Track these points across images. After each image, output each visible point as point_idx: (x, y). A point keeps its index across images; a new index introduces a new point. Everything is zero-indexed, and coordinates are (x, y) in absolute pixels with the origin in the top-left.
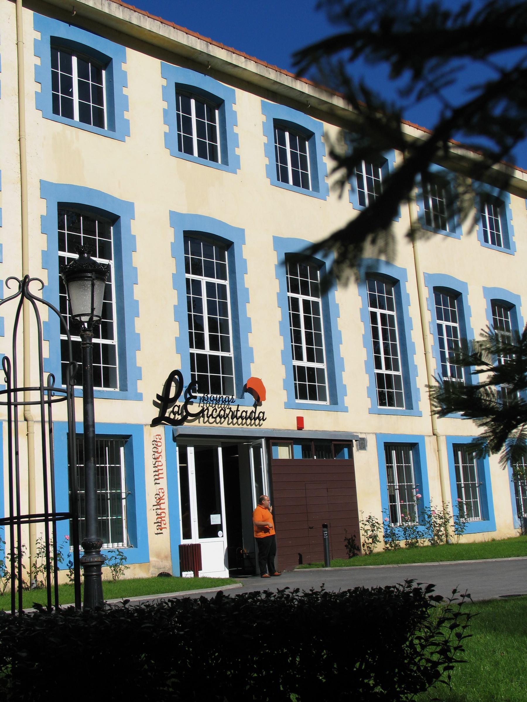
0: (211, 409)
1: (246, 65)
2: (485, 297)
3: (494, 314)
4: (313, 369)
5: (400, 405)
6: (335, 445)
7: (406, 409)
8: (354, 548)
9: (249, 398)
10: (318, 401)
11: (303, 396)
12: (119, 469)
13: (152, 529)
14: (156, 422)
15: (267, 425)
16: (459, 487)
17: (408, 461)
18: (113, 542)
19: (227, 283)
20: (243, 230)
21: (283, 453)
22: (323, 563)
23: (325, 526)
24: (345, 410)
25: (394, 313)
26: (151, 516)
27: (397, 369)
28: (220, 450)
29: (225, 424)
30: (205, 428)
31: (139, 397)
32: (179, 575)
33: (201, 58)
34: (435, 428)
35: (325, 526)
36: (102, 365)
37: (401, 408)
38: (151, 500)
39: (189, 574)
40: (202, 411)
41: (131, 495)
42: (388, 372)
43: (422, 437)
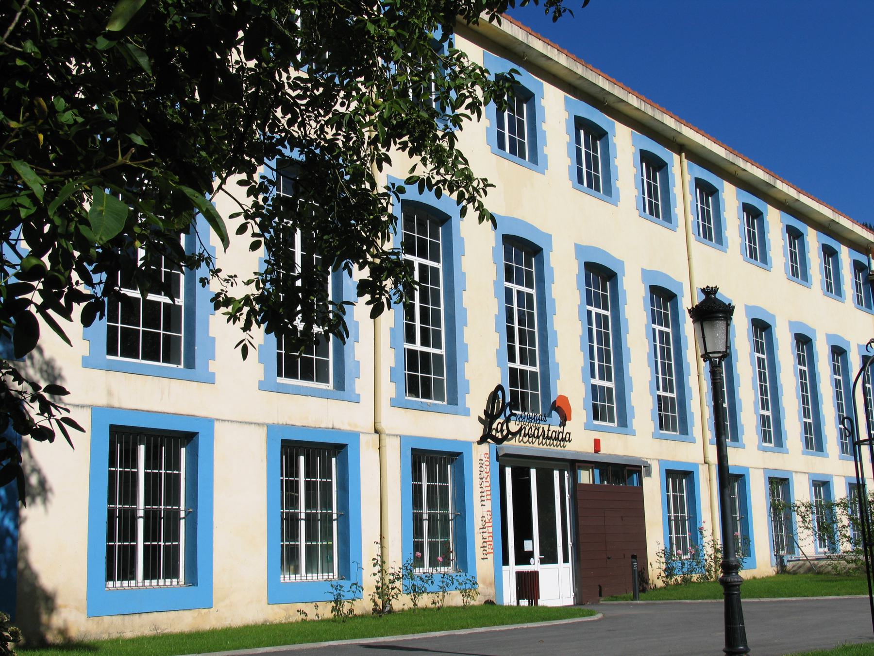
0: (527, 428)
1: (559, 58)
2: (644, 280)
3: (588, 284)
4: (428, 354)
5: (675, 430)
6: (628, 471)
7: (680, 433)
8: (644, 581)
9: (556, 416)
10: (283, 378)
11: (291, 373)
12: (178, 477)
13: (479, 553)
14: (482, 440)
15: (570, 447)
16: (417, 520)
17: (444, 479)
18: (165, 578)
19: (440, 266)
20: (551, 236)
21: (585, 477)
22: (632, 594)
23: (634, 557)
24: (633, 433)
25: (533, 292)
26: (478, 541)
27: (533, 364)
28: (533, 472)
29: (536, 444)
30: (518, 448)
31: (467, 412)
32: (515, 604)
33: (519, 49)
34: (378, 421)
35: (634, 557)
36: (120, 325)
37: (440, 403)
38: (478, 523)
39: (524, 603)
40: (521, 430)
41: (344, 517)
42: (524, 367)
43: (356, 435)
